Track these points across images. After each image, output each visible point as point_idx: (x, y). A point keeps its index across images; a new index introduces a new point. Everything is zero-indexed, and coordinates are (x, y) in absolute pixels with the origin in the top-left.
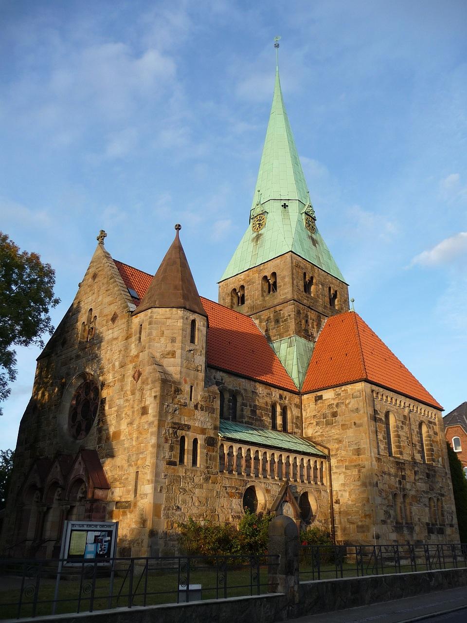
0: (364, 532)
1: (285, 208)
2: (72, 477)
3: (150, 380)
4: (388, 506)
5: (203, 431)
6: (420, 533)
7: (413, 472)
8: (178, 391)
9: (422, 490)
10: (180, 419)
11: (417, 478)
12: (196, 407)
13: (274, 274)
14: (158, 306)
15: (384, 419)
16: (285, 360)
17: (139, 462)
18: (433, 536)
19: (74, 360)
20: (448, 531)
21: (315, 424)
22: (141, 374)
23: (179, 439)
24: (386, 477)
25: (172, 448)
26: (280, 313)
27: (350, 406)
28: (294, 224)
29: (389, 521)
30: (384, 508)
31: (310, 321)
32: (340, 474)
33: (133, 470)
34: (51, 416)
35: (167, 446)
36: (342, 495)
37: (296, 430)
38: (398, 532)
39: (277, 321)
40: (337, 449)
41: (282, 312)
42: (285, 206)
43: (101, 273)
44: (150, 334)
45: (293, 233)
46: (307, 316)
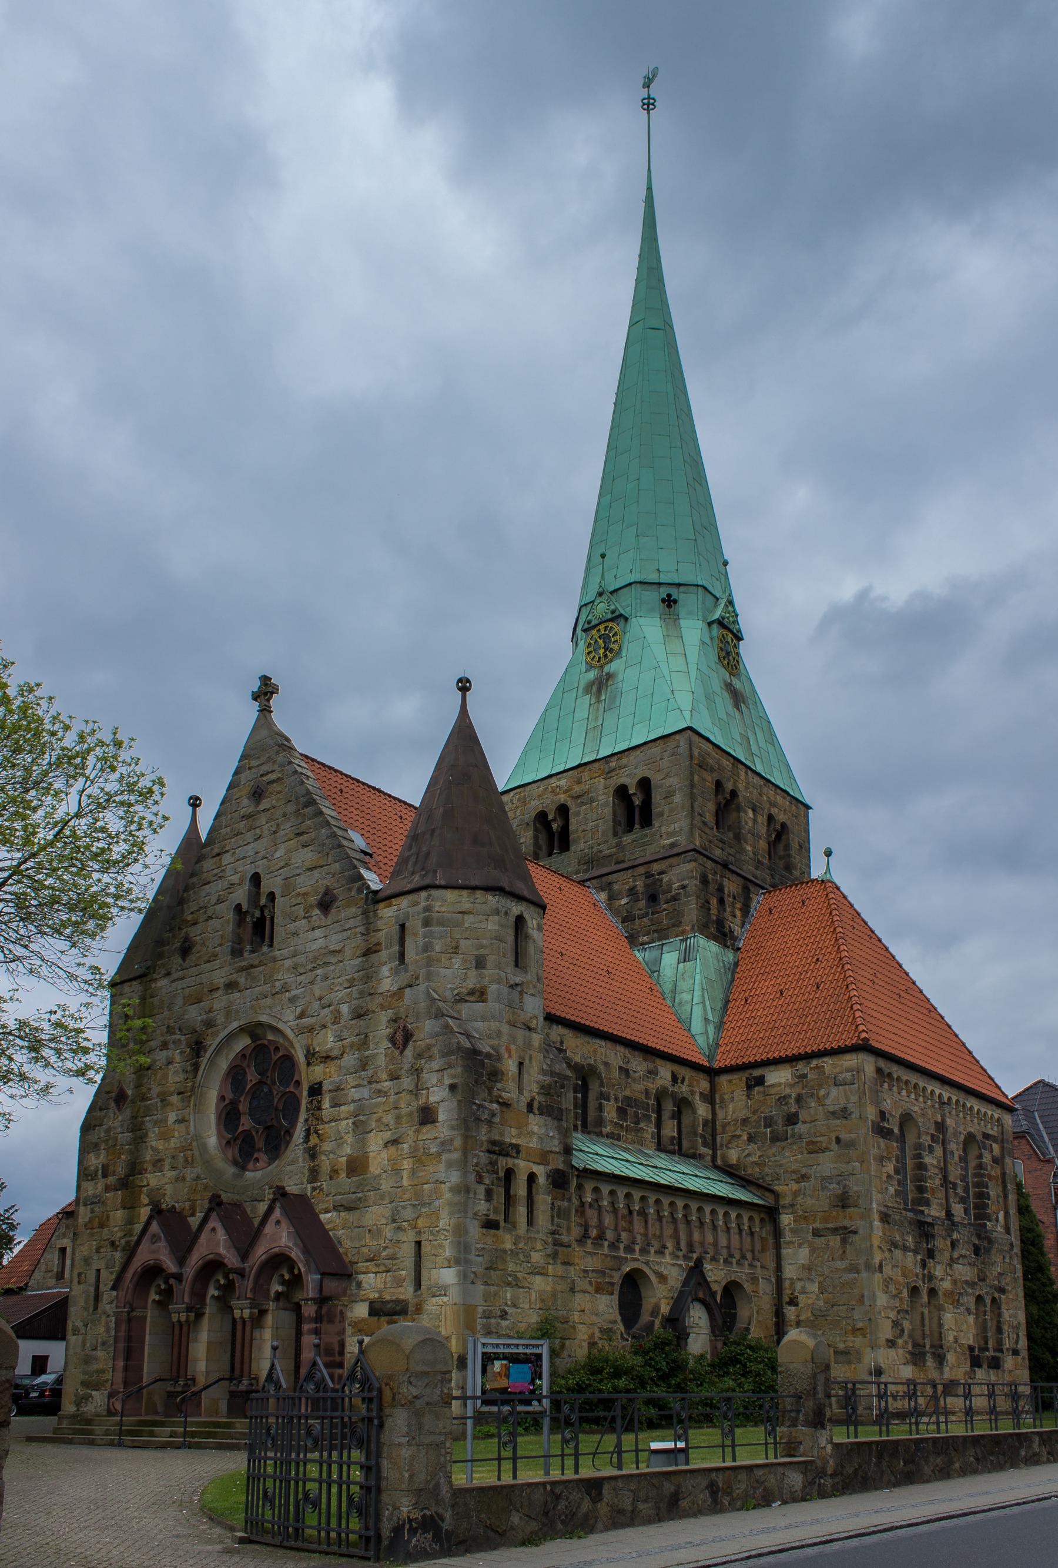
0: (849, 1363)
1: (669, 606)
2: (260, 1252)
3: (435, 1051)
4: (898, 1312)
5: (543, 1157)
6: (956, 1367)
7: (948, 1243)
8: (495, 1075)
9: (964, 1279)
10: (501, 1134)
11: (956, 1255)
12: (530, 1107)
13: (645, 784)
14: (443, 883)
15: (896, 1131)
16: (674, 992)
17: (420, 1223)
18: (980, 1374)
19: (220, 992)
20: (1009, 1362)
21: (745, 1137)
22: (412, 1035)
23: (502, 1174)
24: (898, 1253)
25: (489, 1195)
26: (661, 880)
27: (828, 1101)
28: (693, 652)
29: (900, 1342)
30: (893, 1315)
31: (729, 900)
32: (800, 1246)
33: (409, 1237)
34: (172, 1117)
35: (481, 1190)
36: (804, 1287)
37: (703, 1150)
38: (915, 1364)
39: (653, 898)
40: (796, 1194)
41: (666, 878)
42: (669, 601)
43: (275, 787)
44: (427, 948)
45: (693, 679)
46: (720, 889)
